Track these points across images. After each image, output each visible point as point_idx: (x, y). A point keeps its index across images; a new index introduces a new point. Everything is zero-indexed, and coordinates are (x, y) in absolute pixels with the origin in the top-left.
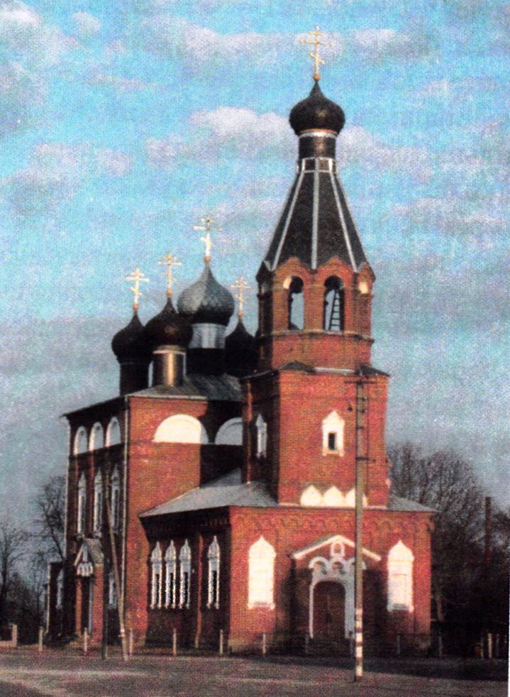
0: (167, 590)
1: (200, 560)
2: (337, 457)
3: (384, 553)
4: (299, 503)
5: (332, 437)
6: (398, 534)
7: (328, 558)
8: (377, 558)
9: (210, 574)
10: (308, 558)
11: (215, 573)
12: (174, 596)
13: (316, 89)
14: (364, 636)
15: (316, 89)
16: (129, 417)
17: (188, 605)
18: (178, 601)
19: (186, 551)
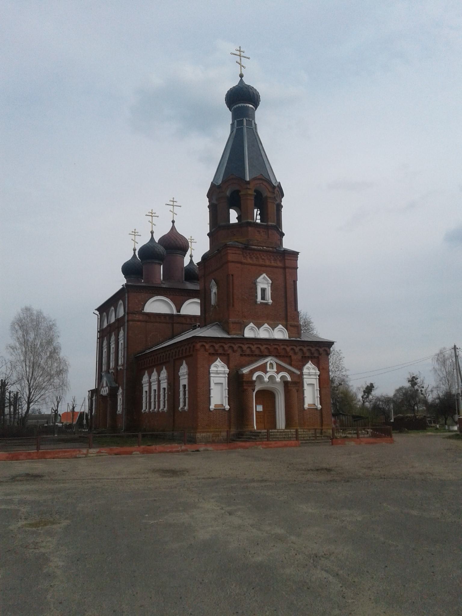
0: (152, 400)
1: (174, 380)
2: (267, 304)
3: (301, 369)
4: (244, 336)
5: (263, 290)
6: (308, 357)
7: (266, 372)
8: (298, 373)
9: (181, 389)
10: (252, 372)
11: (184, 386)
12: (157, 403)
13: (173, 228)
14: (4, 410)
15: (173, 228)
16: (128, 297)
17: (186, 408)
18: (150, 408)
19: (164, 374)
